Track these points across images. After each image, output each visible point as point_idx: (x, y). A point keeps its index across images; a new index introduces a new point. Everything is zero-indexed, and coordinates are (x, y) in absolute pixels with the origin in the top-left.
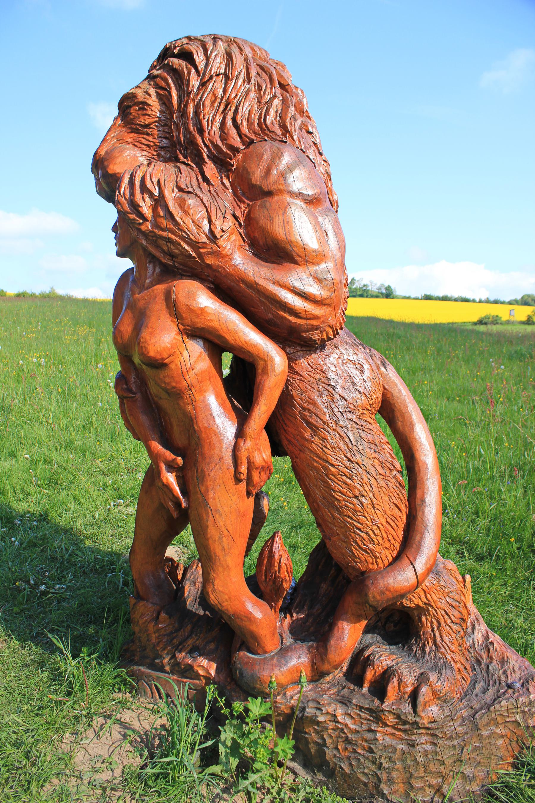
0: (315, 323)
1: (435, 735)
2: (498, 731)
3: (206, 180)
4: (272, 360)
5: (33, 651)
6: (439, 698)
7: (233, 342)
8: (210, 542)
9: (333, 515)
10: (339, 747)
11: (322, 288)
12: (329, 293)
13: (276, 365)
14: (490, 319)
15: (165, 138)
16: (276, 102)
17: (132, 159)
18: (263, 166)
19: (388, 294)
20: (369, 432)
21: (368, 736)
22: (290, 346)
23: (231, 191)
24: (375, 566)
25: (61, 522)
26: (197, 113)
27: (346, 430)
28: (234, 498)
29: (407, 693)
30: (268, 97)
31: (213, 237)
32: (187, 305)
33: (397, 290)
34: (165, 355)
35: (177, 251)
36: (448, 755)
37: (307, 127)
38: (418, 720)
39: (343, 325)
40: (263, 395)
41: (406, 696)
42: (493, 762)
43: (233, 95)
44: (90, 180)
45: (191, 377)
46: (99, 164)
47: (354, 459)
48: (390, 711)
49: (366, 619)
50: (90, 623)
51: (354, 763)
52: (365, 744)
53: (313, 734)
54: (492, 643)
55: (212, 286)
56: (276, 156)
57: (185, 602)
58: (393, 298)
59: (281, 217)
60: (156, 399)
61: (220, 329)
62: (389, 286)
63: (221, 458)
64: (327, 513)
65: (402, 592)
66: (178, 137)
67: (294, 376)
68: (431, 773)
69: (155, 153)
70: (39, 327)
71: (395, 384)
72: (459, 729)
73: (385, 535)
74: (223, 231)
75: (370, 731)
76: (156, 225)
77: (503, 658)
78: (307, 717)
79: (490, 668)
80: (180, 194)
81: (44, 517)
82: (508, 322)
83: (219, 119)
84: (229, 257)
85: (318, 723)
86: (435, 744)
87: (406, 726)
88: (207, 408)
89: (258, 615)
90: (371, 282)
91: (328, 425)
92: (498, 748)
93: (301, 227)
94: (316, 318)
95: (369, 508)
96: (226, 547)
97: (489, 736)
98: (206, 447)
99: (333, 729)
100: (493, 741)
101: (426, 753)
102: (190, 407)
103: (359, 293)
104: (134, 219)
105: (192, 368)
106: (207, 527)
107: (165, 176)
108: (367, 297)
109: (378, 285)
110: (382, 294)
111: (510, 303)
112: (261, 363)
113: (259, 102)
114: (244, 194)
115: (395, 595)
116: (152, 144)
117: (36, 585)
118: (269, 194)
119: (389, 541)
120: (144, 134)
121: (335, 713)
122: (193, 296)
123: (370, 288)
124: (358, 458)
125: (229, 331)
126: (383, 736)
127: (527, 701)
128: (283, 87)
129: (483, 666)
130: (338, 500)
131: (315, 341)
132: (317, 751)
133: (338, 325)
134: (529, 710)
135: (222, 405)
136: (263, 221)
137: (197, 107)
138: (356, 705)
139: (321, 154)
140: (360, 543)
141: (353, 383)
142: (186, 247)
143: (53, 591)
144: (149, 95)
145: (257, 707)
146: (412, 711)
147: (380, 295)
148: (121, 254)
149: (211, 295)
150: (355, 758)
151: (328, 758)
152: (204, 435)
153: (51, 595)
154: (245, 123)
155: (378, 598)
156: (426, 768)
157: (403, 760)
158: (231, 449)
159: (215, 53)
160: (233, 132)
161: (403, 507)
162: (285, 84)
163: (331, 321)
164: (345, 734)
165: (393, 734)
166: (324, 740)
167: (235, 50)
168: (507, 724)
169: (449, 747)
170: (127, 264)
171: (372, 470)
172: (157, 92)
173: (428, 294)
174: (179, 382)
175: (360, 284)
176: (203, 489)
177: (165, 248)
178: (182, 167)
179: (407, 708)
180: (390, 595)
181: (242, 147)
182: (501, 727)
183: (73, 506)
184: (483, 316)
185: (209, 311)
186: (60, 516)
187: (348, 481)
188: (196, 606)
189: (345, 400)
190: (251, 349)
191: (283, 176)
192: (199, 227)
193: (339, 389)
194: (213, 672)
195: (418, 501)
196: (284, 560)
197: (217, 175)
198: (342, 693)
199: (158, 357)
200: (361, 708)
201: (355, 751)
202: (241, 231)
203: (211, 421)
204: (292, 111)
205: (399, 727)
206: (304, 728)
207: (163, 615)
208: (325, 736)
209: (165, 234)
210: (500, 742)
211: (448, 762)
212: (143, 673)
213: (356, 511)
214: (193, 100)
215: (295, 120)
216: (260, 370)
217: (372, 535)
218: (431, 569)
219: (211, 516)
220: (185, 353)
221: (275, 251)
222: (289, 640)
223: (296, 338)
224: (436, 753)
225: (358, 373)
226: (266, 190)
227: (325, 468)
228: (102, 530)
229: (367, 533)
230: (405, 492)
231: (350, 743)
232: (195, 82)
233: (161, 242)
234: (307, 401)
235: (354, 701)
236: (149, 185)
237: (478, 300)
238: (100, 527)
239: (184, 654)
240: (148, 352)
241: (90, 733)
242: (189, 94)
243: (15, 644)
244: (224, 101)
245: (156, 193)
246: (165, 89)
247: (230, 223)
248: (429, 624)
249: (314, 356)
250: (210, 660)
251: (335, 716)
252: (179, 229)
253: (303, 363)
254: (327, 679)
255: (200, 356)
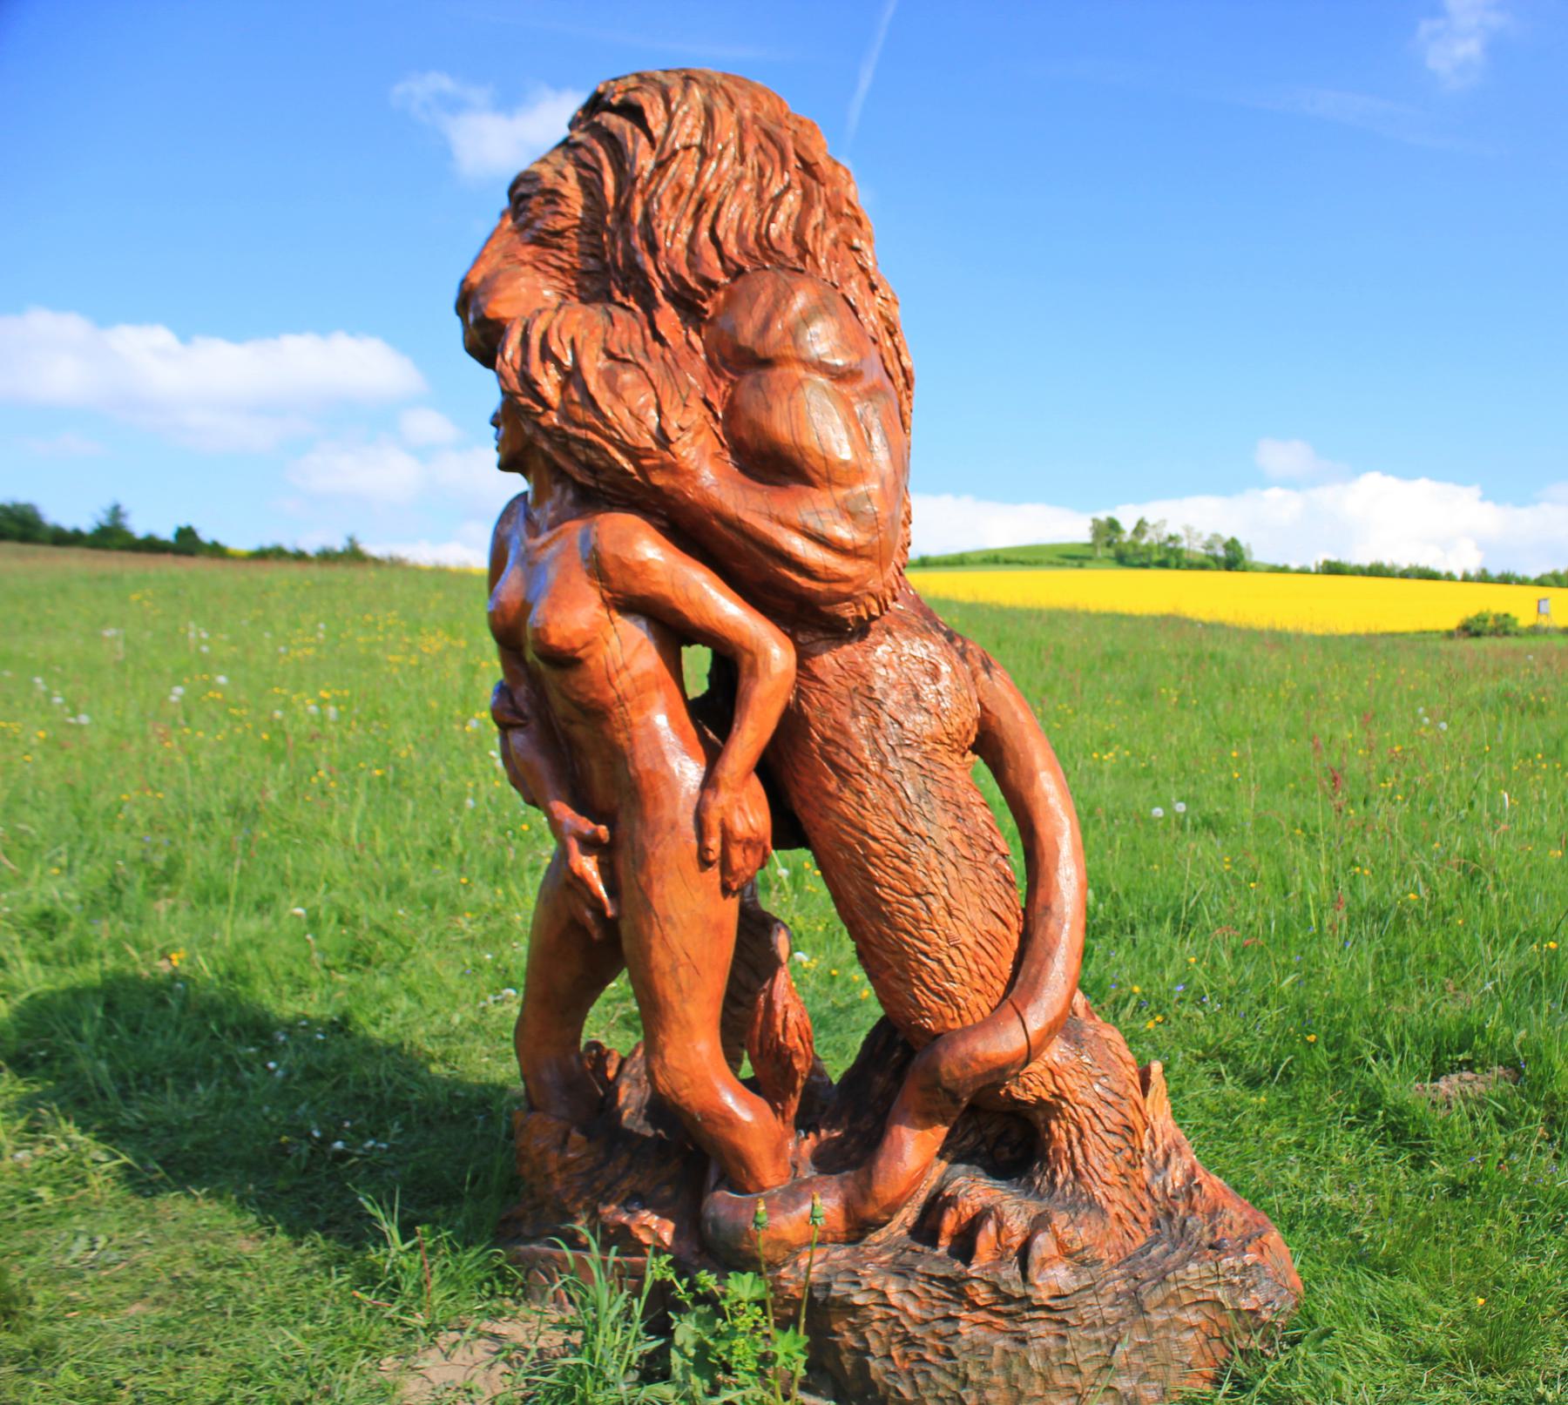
0: (843, 588)
1: (1063, 1322)
2: (1183, 1317)
3: (658, 337)
4: (766, 652)
5: (318, 1244)
6: (1070, 1255)
7: (696, 621)
8: (656, 976)
9: (879, 931)
10: (894, 1354)
11: (856, 527)
12: (868, 537)
13: (773, 662)
14: (1490, 624)
15: (593, 256)
16: (790, 197)
17: (530, 294)
18: (759, 313)
19: (1232, 559)
20: (946, 782)
21: (943, 1328)
22: (803, 631)
23: (703, 357)
24: (958, 1025)
25: (377, 1033)
26: (647, 216)
27: (898, 776)
28: (699, 896)
29: (1011, 1247)
30: (775, 190)
31: (663, 439)
32: (616, 557)
33: (1253, 549)
34: (578, 643)
35: (602, 463)
36: (1085, 1355)
37: (850, 238)
38: (1030, 1291)
39: (898, 594)
40: (749, 713)
41: (1011, 1252)
42: (1173, 1374)
43: (712, 187)
44: (453, 329)
45: (623, 683)
46: (466, 300)
47: (914, 828)
48: (980, 1279)
49: (945, 1123)
50: (436, 1202)
51: (919, 1380)
52: (940, 1344)
53: (847, 1334)
54: (1199, 1185)
55: (664, 524)
56: (786, 295)
57: (619, 1114)
58: (1244, 570)
59: (785, 406)
60: (564, 725)
61: (673, 597)
62: (1234, 541)
63: (674, 825)
64: (870, 929)
65: (1000, 1062)
66: (614, 258)
67: (811, 684)
68: (1057, 1389)
69: (572, 283)
70: (321, 635)
71: (1007, 703)
72: (1107, 1311)
73: (973, 967)
74: (682, 429)
75: (949, 1318)
76: (567, 417)
77: (1216, 1208)
78: (834, 1299)
79: (1189, 1223)
80: (608, 364)
81: (341, 1026)
82: (1534, 630)
83: (687, 228)
84: (694, 475)
85: (855, 1309)
86: (1062, 1337)
87: (1012, 1306)
88: (654, 734)
89: (745, 1116)
90: (1188, 529)
91: (868, 770)
92: (1183, 1347)
93: (823, 424)
94: (846, 579)
95: (942, 915)
96: (684, 985)
97: (1165, 1326)
98: (649, 806)
99: (881, 1320)
100: (1173, 1335)
101: (1046, 1353)
102: (622, 737)
103: (1156, 557)
104: (528, 406)
105: (626, 667)
106: (650, 948)
107: (584, 333)
108: (1178, 567)
109: (1206, 537)
110: (1216, 559)
111: (1540, 582)
112: (747, 658)
113: (759, 198)
114: (725, 362)
115: (986, 1068)
116: (567, 266)
117: (326, 1141)
118: (767, 363)
119: (982, 977)
120: (552, 247)
121: (883, 1286)
122: (627, 540)
123: (1184, 544)
124: (920, 826)
125: (690, 602)
126: (969, 1329)
127: (1239, 1265)
128: (808, 168)
129: (1176, 1221)
130: (888, 903)
131: (846, 620)
132: (854, 1365)
133: (889, 593)
134: (1242, 1281)
135: (680, 732)
136: (755, 412)
137: (647, 205)
138: (923, 1274)
139: (873, 288)
140: (928, 980)
141: (917, 696)
142: (619, 457)
143: (359, 1152)
144: (564, 177)
145: (743, 1287)
146: (1019, 1277)
147: (1211, 562)
148: (505, 466)
149: (662, 538)
150: (922, 1371)
151: (873, 1376)
152: (645, 785)
153: (355, 1160)
154: (732, 237)
155: (957, 1073)
156: (1046, 1380)
157: (1006, 1368)
158: (692, 809)
159: (685, 108)
160: (710, 254)
161: (1012, 920)
162: (811, 161)
163: (874, 584)
164: (902, 1326)
165: (988, 1324)
166: (863, 1339)
167: (721, 104)
168: (1201, 1306)
169: (1089, 1341)
170: (517, 484)
171: (947, 848)
172: (579, 175)
173: (1333, 558)
174: (603, 692)
175: (1158, 535)
176: (643, 879)
177: (582, 458)
178: (617, 312)
179: (1011, 1272)
180: (978, 1069)
181: (723, 280)
182: (1190, 1311)
183: (404, 1003)
184: (1471, 615)
185: (657, 567)
186: (377, 1024)
187: (904, 867)
188: (641, 1122)
189: (901, 725)
190: (729, 634)
191: (793, 332)
192: (639, 420)
193: (889, 704)
194: (667, 1236)
195: (1038, 909)
196: (792, 1016)
197: (680, 328)
198: (901, 1259)
199: (566, 646)
200: (931, 1278)
201: (922, 1360)
202: (718, 429)
203: (658, 760)
204: (818, 215)
205: (999, 1308)
206: (830, 1324)
207: (576, 1135)
208: (868, 1335)
209: (581, 433)
210: (1188, 1336)
211: (1087, 1369)
212: (536, 1255)
213: (917, 920)
214: (642, 192)
215: (825, 229)
216: (744, 671)
217: (949, 965)
218: (1064, 1026)
219: (656, 928)
220: (614, 640)
221: (772, 463)
222: (808, 1171)
223: (811, 616)
224: (1065, 1352)
225: (928, 680)
226: (762, 355)
227: (863, 845)
228: (467, 1045)
229: (939, 961)
230: (1022, 890)
231: (913, 1344)
232: (645, 161)
233: (575, 447)
234: (833, 728)
235: (919, 1268)
236: (555, 348)
237: (1459, 576)
238: (462, 1040)
239: (613, 1207)
240: (548, 638)
241: (435, 1354)
242: (634, 182)
243: (282, 1240)
244: (696, 196)
245: (568, 361)
246: (594, 170)
247: (697, 413)
248: (1063, 1135)
249: (847, 648)
250: (663, 1216)
251: (884, 1294)
252: (605, 425)
253: (828, 661)
254: (875, 1237)
255: (640, 646)
